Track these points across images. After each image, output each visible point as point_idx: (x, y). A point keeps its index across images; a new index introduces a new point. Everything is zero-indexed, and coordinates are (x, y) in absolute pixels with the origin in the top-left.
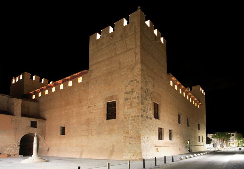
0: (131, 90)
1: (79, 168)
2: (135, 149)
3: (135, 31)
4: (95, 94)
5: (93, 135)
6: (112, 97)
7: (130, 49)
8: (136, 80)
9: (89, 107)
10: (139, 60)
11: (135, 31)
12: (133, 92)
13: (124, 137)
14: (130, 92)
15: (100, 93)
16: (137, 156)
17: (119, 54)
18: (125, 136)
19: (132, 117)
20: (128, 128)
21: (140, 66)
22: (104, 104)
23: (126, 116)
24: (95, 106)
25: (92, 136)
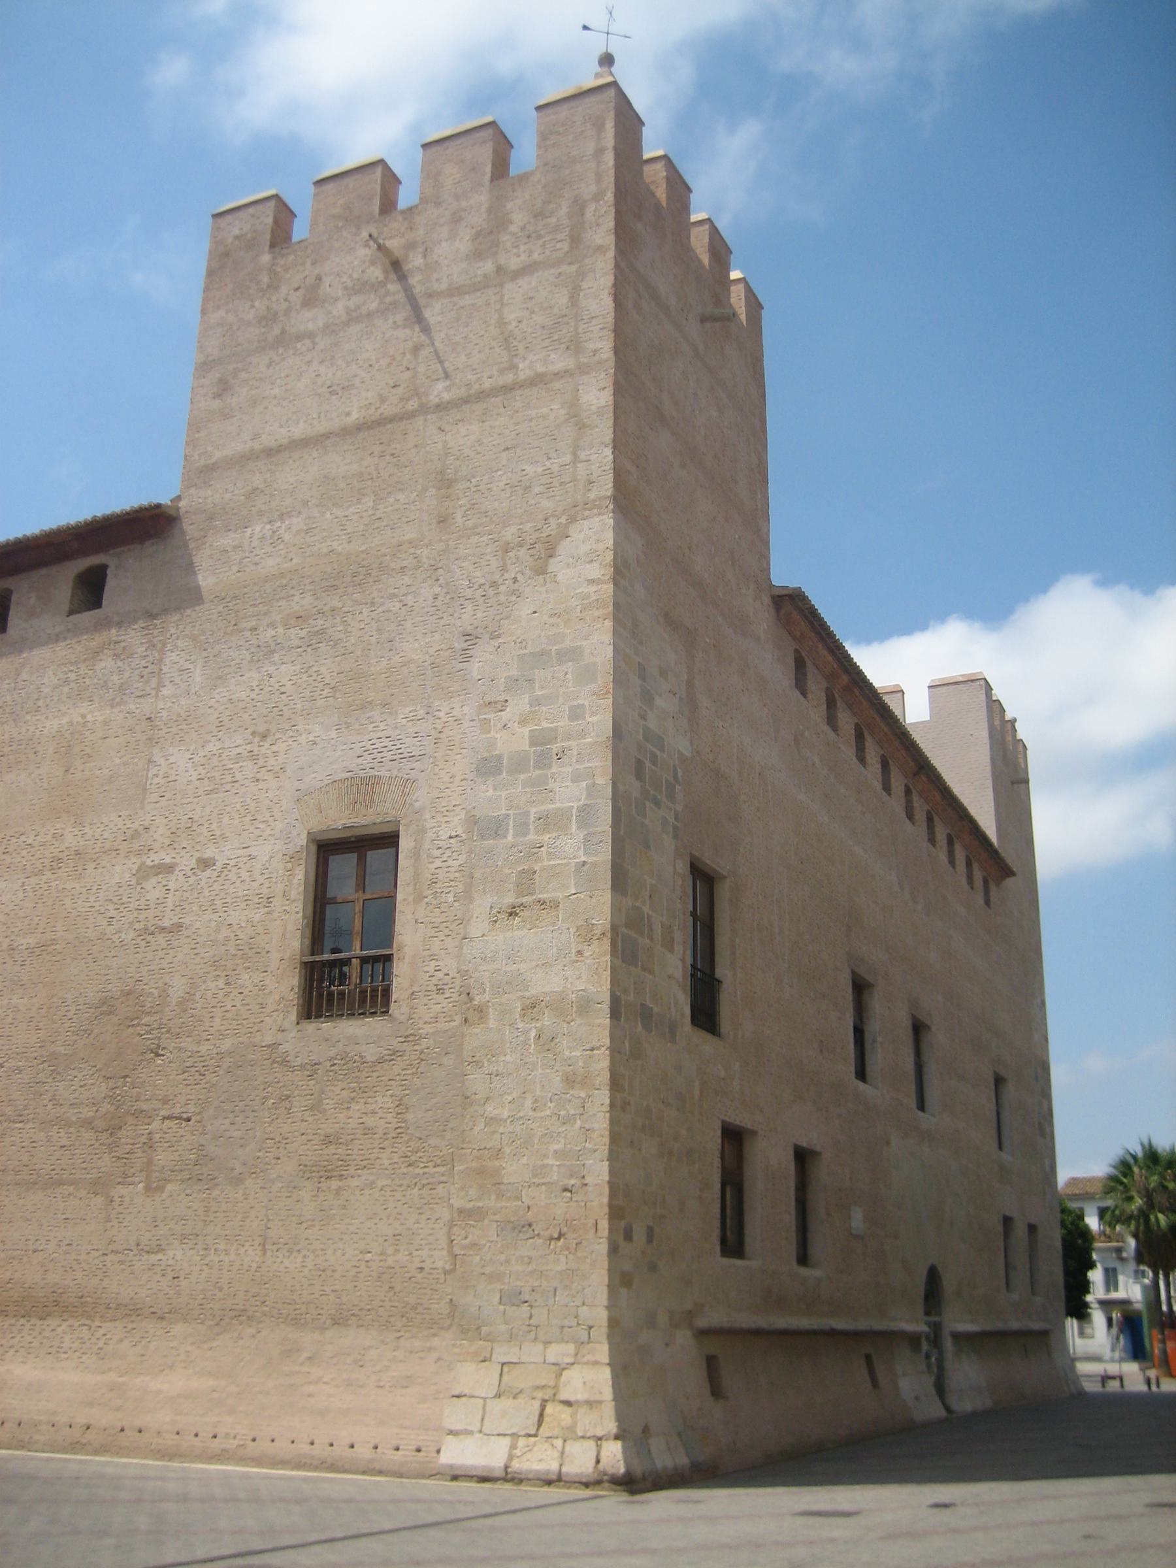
0: (533, 743)
1: (101, 563)
2: (551, 1358)
3: (575, 240)
4: (214, 746)
5: (160, 1189)
6: (363, 787)
7: (538, 380)
8: (567, 655)
9: (144, 873)
10: (606, 487)
11: (575, 240)
12: (542, 761)
13: (451, 1225)
14: (519, 764)
15: (264, 737)
16: (569, 1434)
17: (440, 407)
18: (461, 1211)
19: (532, 1008)
20: (492, 1120)
21: (609, 538)
22: (1136, 1272)
23: (477, 1000)
24: (206, 864)
25: (148, 1189)
